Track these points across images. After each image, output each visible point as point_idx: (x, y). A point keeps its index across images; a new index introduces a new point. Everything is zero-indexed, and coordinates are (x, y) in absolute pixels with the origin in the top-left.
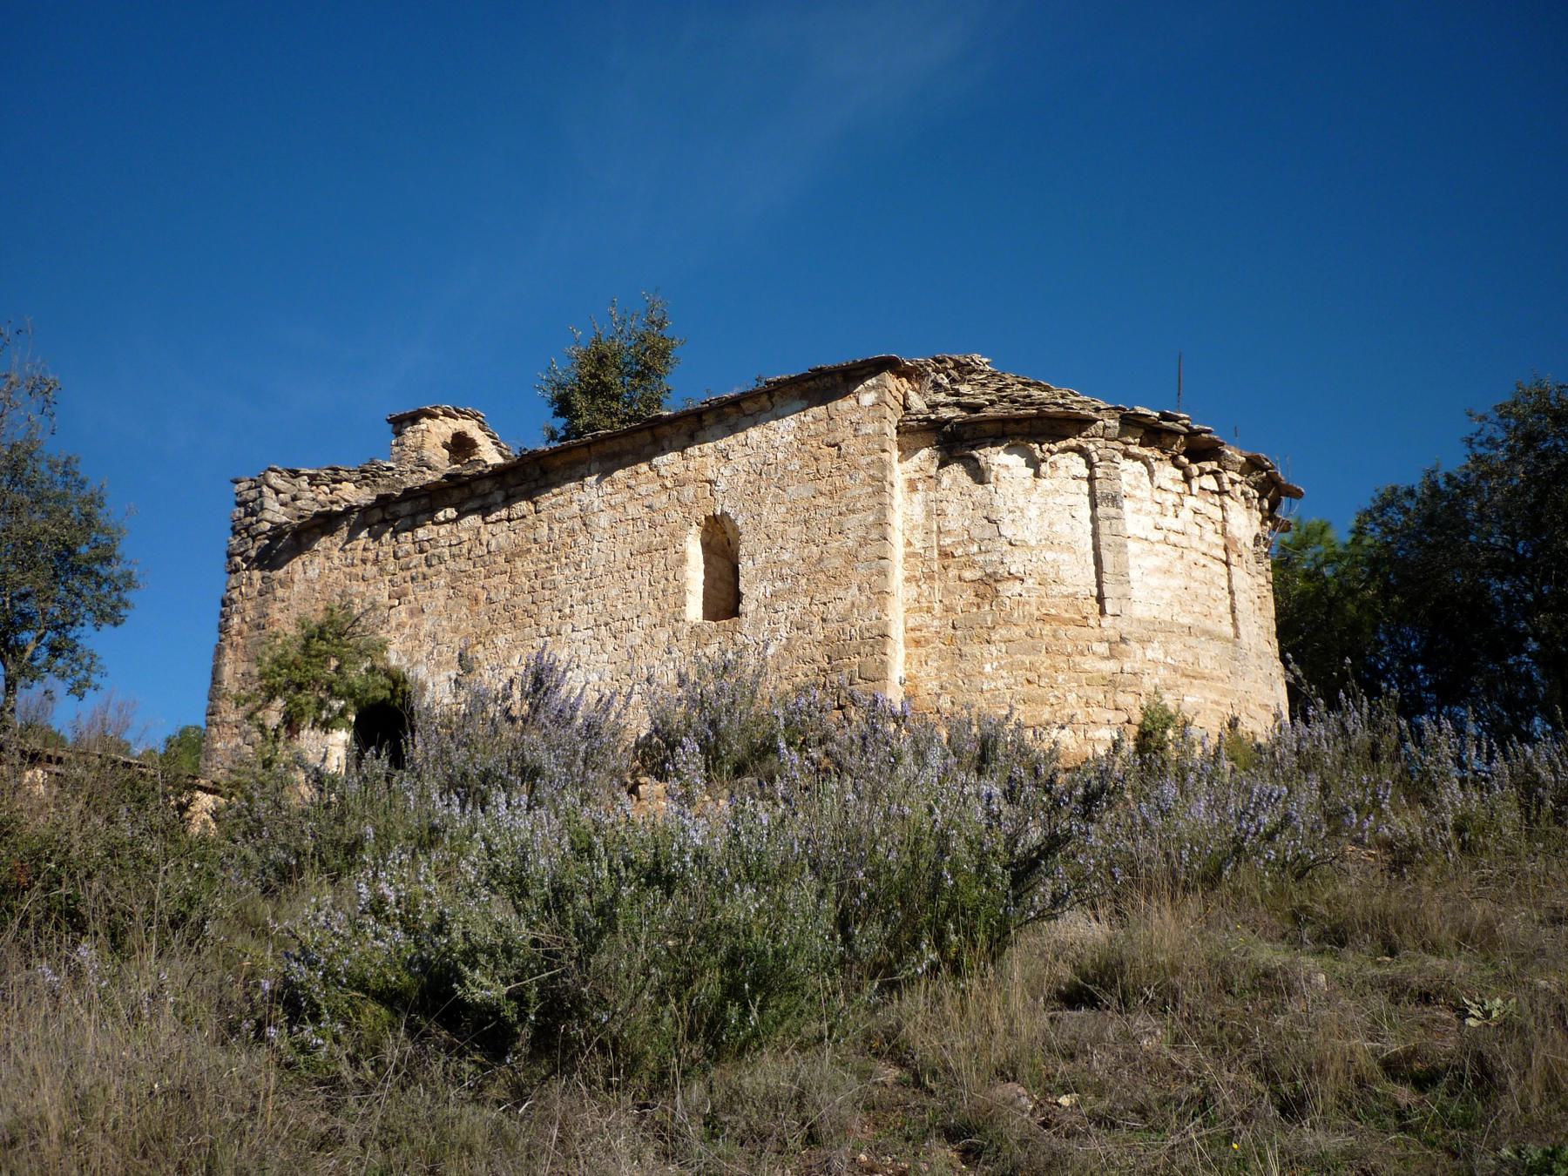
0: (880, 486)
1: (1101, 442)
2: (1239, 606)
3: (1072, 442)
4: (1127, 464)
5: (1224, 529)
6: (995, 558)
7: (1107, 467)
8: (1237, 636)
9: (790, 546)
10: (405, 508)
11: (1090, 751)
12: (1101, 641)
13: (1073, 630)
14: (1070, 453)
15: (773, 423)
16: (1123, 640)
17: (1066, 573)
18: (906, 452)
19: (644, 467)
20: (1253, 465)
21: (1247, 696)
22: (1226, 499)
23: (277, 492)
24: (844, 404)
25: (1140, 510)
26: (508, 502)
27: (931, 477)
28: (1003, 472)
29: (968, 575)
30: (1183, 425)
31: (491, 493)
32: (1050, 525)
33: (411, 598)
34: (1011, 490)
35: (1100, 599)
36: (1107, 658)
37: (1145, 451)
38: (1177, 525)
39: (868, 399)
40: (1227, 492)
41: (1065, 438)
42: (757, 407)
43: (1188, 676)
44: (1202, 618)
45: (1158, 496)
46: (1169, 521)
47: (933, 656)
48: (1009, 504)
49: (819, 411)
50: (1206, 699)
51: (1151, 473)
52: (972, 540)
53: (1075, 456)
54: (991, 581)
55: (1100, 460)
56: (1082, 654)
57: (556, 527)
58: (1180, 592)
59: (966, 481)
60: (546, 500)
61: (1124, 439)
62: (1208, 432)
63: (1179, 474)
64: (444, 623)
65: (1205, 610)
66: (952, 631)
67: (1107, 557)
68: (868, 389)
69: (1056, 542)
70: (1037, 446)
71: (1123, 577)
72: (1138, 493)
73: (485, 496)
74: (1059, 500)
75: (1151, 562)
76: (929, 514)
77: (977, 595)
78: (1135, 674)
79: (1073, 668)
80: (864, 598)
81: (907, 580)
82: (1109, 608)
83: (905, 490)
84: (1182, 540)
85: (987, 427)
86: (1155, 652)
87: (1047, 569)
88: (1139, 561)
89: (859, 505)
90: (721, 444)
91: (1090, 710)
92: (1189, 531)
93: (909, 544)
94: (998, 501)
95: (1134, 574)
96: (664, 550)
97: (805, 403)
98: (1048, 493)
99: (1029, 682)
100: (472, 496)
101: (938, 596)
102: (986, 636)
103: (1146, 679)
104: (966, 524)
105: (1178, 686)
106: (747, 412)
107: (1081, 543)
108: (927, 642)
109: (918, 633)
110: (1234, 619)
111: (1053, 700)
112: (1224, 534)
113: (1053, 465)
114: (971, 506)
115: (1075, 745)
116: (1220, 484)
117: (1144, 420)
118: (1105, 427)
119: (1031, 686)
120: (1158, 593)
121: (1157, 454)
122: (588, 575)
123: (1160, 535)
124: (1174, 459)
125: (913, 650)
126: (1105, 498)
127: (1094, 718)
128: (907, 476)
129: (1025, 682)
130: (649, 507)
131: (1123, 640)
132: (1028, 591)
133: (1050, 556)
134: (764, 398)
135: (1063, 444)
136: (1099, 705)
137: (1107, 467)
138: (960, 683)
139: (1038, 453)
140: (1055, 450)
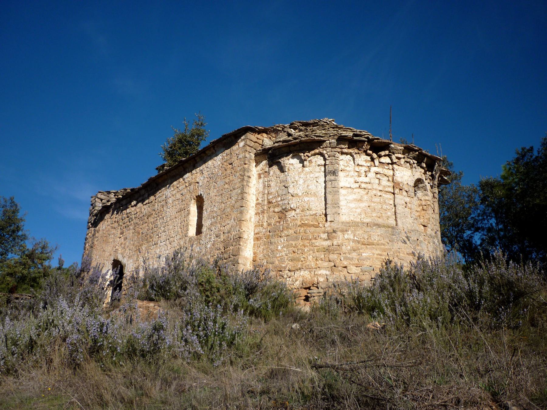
0: (244, 177)
1: (329, 149)
2: (398, 211)
3: (317, 151)
4: (343, 157)
5: (393, 179)
6: (286, 202)
7: (332, 159)
8: (397, 225)
9: (216, 205)
10: (124, 202)
11: (316, 279)
12: (324, 233)
13: (313, 229)
14: (317, 156)
15: (216, 158)
16: (334, 232)
17: (313, 206)
18: (258, 163)
19: (181, 180)
20: (408, 150)
21: (400, 250)
22: (395, 166)
23: (101, 200)
24: (235, 147)
25: (348, 175)
26: (148, 198)
27: (266, 172)
28: (291, 167)
29: (277, 210)
30: (365, 138)
31: (145, 194)
32: (308, 186)
33: (125, 234)
34: (293, 174)
35: (326, 215)
36: (326, 240)
37: (350, 151)
38: (367, 180)
39: (242, 144)
40: (395, 163)
41: (313, 149)
42: (210, 152)
43: (365, 244)
44: (376, 219)
45: (357, 169)
46: (363, 179)
47: (262, 244)
48: (293, 179)
49: (228, 151)
50: (373, 254)
51: (354, 159)
52: (279, 196)
53: (319, 156)
54: (284, 212)
55: (329, 157)
56: (316, 239)
57: (159, 204)
58: (365, 209)
59: (278, 172)
60: (158, 194)
62: (378, 139)
63: (369, 158)
64: (131, 242)
65: (379, 215)
66: (269, 233)
67: (329, 197)
68: (242, 141)
69: (309, 193)
70: (302, 154)
71: (336, 205)
72: (348, 168)
73: (143, 195)
74: (311, 176)
75: (352, 197)
76: (264, 186)
77: (279, 218)
78: (339, 246)
79: (312, 245)
80: (235, 223)
81: (256, 214)
82: (329, 219)
83: (257, 178)
84: (369, 186)
85: (283, 149)
86: (349, 235)
87: (305, 204)
88: (346, 197)
89: (236, 186)
90: (201, 168)
91: (318, 262)
92: (372, 181)
93: (257, 199)
94: (289, 179)
95: (342, 203)
96: (184, 211)
97: (224, 148)
98: (307, 173)
99: (294, 252)
100: (140, 196)
101: (266, 219)
102: (280, 235)
103: (344, 247)
104: (277, 189)
105: (359, 249)
106: (209, 155)
107: (320, 192)
108: (261, 238)
109: (258, 235)
110: (396, 217)
111: (302, 259)
112: (393, 181)
113: (310, 162)
114: (279, 182)
115: (310, 278)
116: (392, 160)
117: (345, 138)
118: (330, 143)
119: (294, 254)
120: (354, 210)
121: (356, 151)
122: (165, 222)
124: (365, 152)
125: (256, 242)
126: (330, 172)
127: (319, 265)
128: (258, 173)
129: (292, 253)
130: (182, 194)
131: (334, 232)
132: (297, 214)
133: (306, 199)
134: (212, 149)
135: (313, 152)
136: (322, 260)
137: (332, 159)
138: (270, 254)
139: (303, 158)
140: (309, 155)
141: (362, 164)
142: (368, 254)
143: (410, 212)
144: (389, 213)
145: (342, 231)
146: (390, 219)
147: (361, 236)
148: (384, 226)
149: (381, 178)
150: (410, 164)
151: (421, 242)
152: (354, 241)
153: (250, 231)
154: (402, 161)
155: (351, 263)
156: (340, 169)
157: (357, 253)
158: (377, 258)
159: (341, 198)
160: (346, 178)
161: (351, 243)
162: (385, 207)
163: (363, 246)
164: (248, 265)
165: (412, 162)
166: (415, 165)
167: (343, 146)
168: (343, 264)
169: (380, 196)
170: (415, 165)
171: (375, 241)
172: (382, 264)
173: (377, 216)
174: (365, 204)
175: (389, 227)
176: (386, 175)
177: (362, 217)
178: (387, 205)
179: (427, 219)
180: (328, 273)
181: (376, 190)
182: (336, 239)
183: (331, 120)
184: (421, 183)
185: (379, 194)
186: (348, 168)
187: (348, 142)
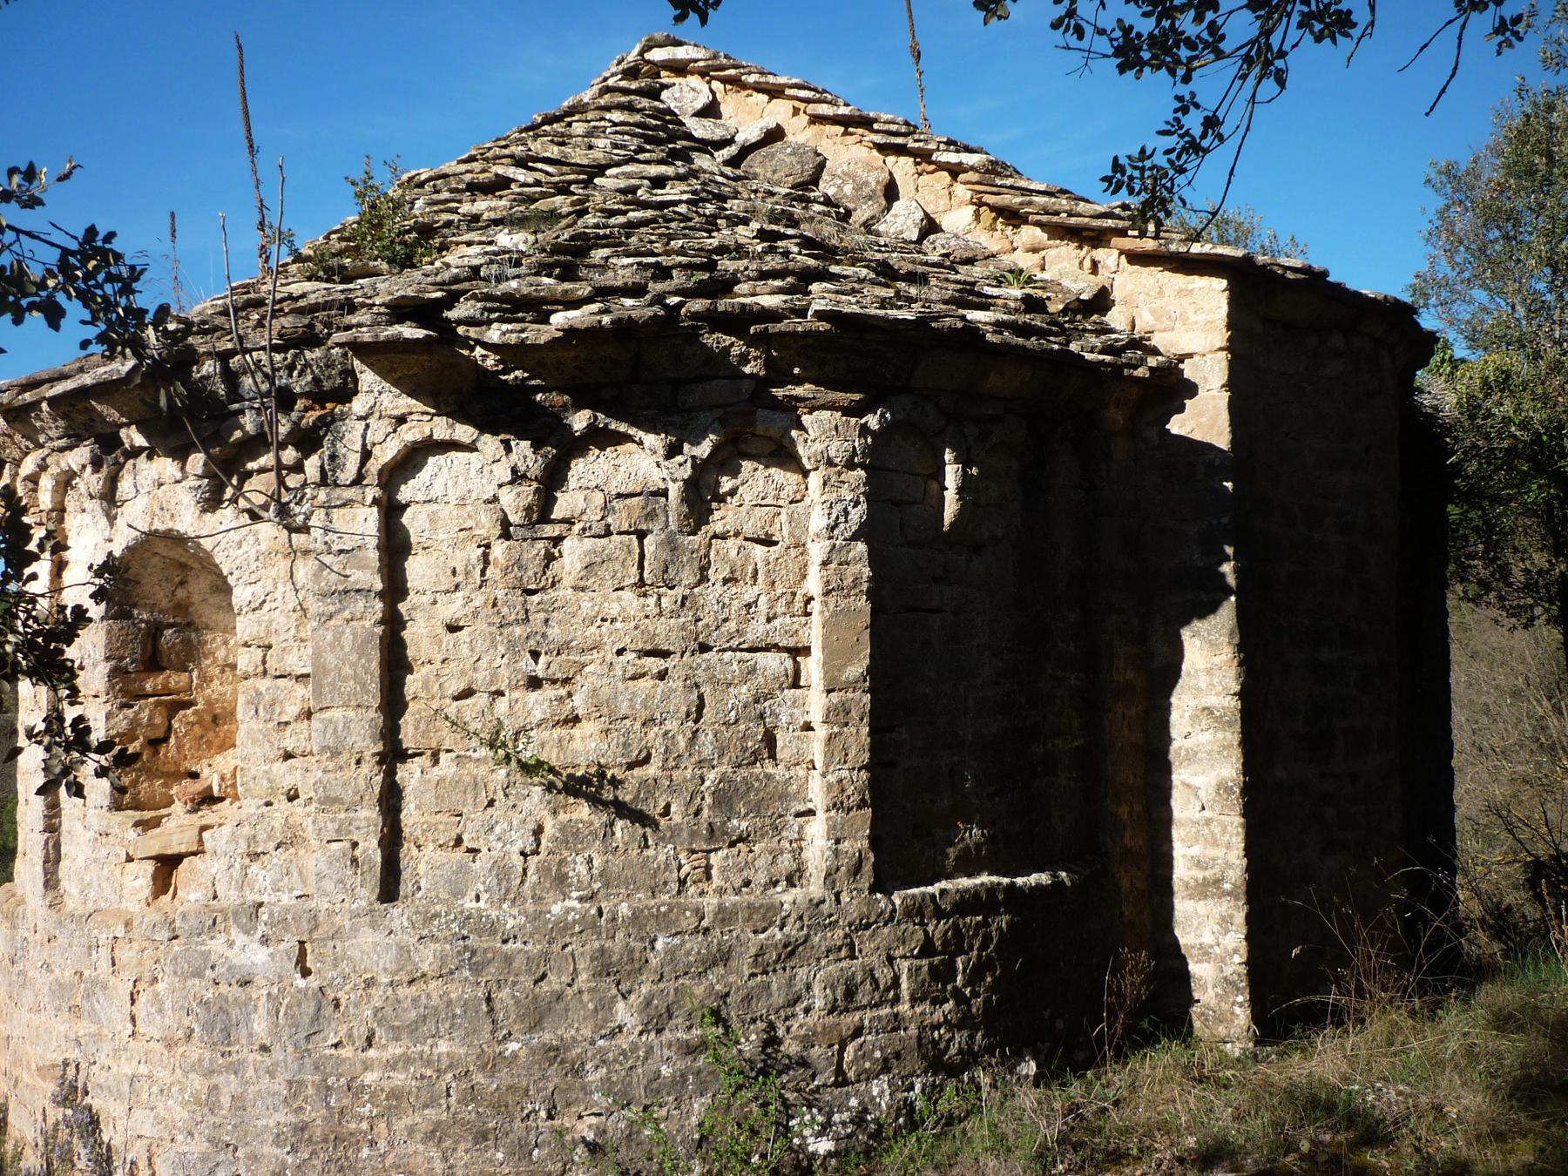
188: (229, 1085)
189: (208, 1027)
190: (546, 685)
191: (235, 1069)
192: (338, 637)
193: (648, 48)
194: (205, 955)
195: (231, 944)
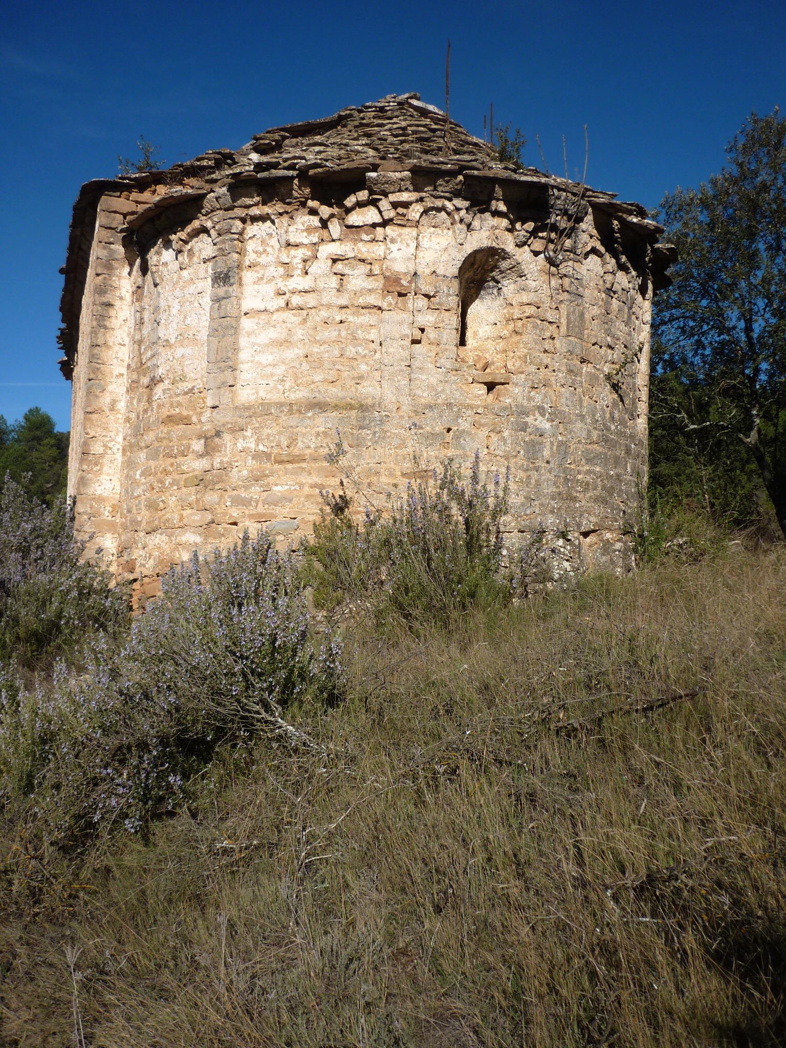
3: (196, 224)
36: (202, 456)
37: (267, 210)
38: (304, 283)
41: (189, 221)
43: (281, 462)
50: (301, 485)
61: (239, 202)
65: (332, 375)
84: (311, 300)
86: (247, 441)
88: (253, 339)
92: (321, 285)
120: (270, 370)
121: (280, 207)
123: (281, 302)
135: (189, 229)
141: (298, 241)
142: (287, 487)
143: (433, 354)
144: (364, 368)
145: (233, 431)
146: (365, 383)
147: (272, 441)
148: (336, 407)
149: (346, 271)
150: (449, 214)
151: (461, 434)
152: (257, 456)
153: (112, 434)
154: (415, 212)
155: (247, 512)
156: (247, 263)
157: (261, 486)
158: (308, 497)
159: (243, 342)
160: (256, 287)
161: (250, 461)
162: (351, 351)
163: (276, 466)
164: (107, 514)
165: (449, 205)
166: (463, 212)
167: (248, 201)
168: (231, 516)
169: (341, 322)
170: (463, 212)
171: (308, 451)
172: (321, 510)
173: (324, 381)
174: (296, 351)
175: (351, 407)
176: (363, 261)
177: (287, 386)
178: (361, 345)
179: (520, 358)
180: (198, 539)
181: (329, 306)
182: (220, 451)
183: (406, 95)
184: (504, 259)
185: (338, 318)
186: (263, 259)
187: (253, 188)
188: (535, 475)
189: (527, 452)
190: (397, 336)
191: (537, 469)
192: (574, 310)
193: (411, 98)
194: (526, 423)
195: (162, 432)
